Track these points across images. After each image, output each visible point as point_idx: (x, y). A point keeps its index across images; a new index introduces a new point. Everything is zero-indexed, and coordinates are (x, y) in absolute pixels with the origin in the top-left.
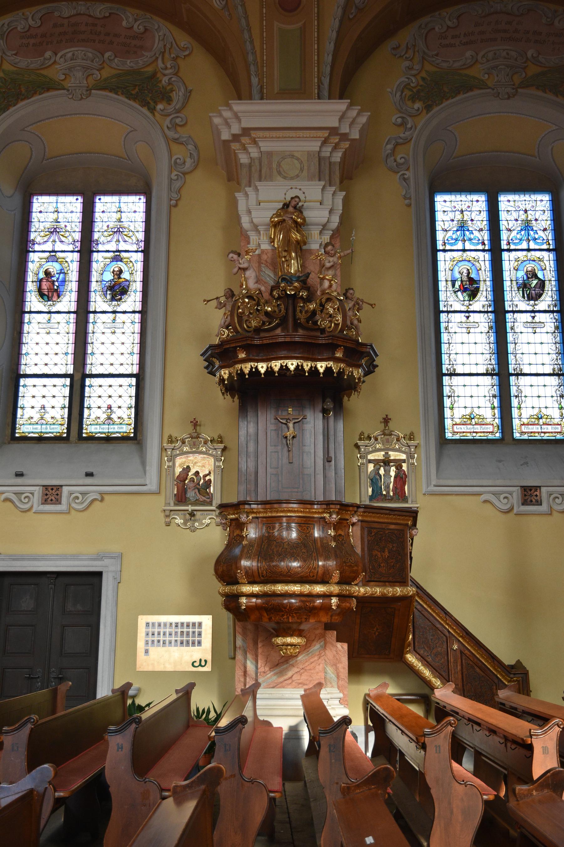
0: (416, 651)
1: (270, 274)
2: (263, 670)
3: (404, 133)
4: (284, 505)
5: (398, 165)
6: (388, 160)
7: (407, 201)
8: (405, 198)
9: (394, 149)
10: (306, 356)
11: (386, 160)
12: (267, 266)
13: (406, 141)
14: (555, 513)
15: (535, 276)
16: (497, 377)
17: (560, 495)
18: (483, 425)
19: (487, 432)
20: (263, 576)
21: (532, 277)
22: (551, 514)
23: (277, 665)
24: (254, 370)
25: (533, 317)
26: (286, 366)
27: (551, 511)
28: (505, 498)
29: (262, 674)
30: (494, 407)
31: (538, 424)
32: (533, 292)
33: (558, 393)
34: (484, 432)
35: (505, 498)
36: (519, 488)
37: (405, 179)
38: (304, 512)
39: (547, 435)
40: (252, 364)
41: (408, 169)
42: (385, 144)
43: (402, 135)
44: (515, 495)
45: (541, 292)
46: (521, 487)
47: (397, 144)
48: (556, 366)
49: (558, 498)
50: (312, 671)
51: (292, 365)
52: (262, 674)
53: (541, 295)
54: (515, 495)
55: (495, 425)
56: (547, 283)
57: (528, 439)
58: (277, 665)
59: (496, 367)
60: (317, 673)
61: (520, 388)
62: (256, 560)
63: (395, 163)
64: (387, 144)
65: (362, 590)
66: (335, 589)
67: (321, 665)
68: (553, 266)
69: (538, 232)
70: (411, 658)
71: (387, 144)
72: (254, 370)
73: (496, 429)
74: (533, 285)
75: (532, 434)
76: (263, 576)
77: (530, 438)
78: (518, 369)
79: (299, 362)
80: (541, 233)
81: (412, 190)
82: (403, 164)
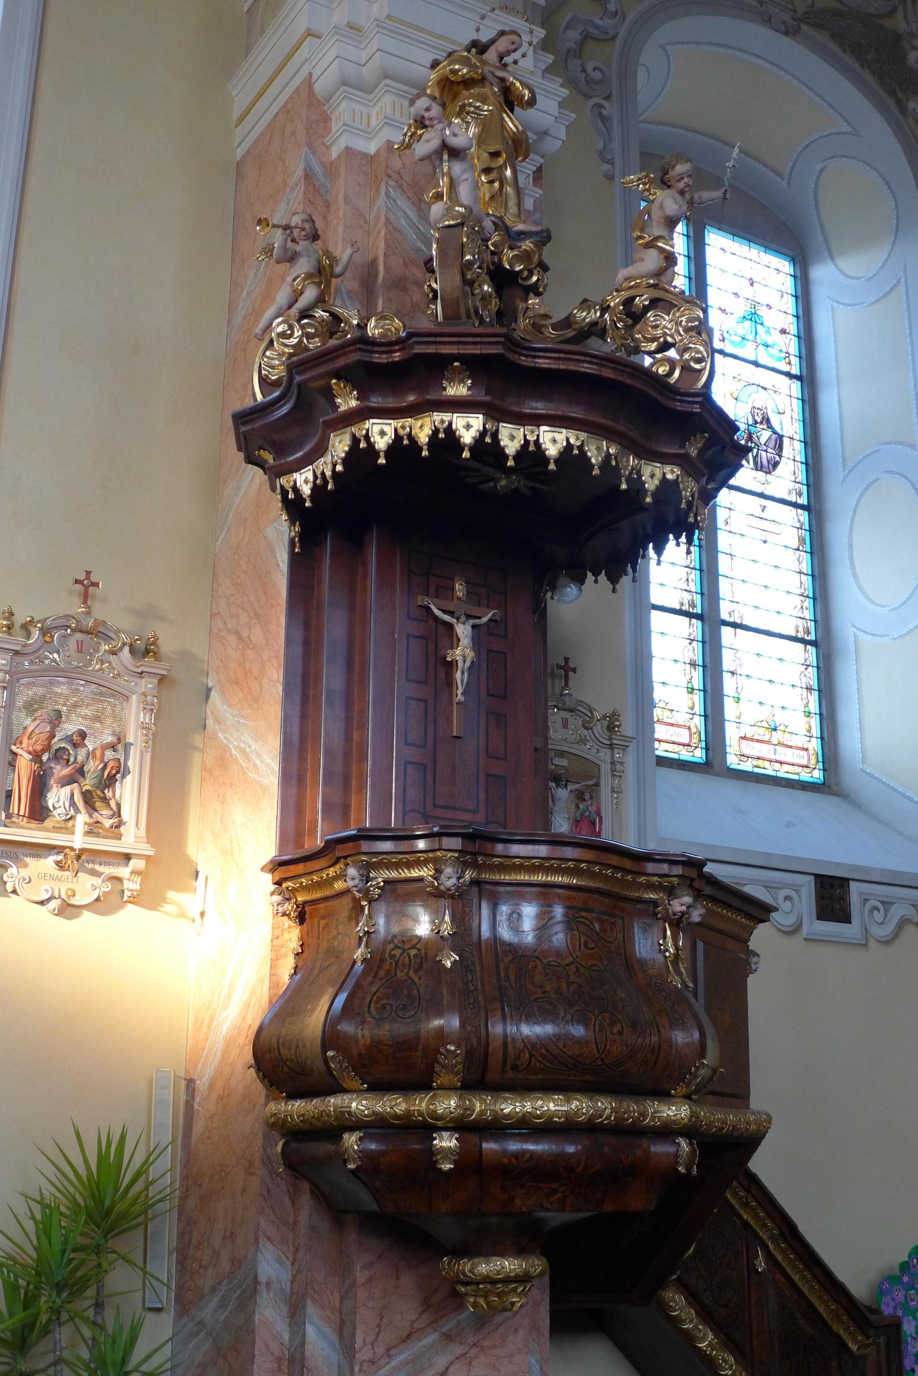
0: (684, 1286)
1: (409, 213)
2: (370, 1355)
3: (601, 19)
4: (500, 848)
5: (589, 80)
6: (570, 62)
7: (606, 167)
8: (603, 159)
9: (582, 44)
10: (594, 418)
11: (566, 62)
12: (401, 187)
13: (606, 37)
14: (872, 944)
15: (767, 421)
16: (700, 623)
17: (882, 902)
18: (672, 725)
19: (680, 744)
20: (515, 1068)
21: (761, 423)
22: (865, 945)
23: (409, 1336)
24: (442, 435)
25: (764, 508)
26: (537, 442)
27: (867, 940)
28: (787, 898)
29: (365, 1365)
30: (693, 689)
31: (768, 742)
32: (764, 454)
33: (804, 680)
34: (673, 743)
35: (787, 898)
36: (812, 878)
37: (603, 118)
38: (589, 874)
39: (786, 768)
40: (438, 417)
41: (608, 98)
42: (563, 26)
43: (597, 21)
44: (804, 892)
45: (777, 458)
46: (817, 876)
47: (586, 37)
48: (800, 622)
49: (878, 910)
50: (498, 1352)
51: (553, 441)
52: (365, 1365)
53: (776, 465)
54: (804, 892)
55: (694, 730)
56: (786, 441)
57: (753, 773)
58: (409, 1336)
59: (698, 599)
60: (512, 1355)
61: (738, 655)
62: (499, 1013)
63: (584, 75)
64: (568, 27)
65: (552, 1106)
66: (448, 1104)
67: (521, 1331)
68: (796, 410)
69: (772, 331)
70: (677, 1302)
71: (568, 27)
72: (442, 435)
73: (695, 740)
74: (763, 440)
75: (760, 763)
76: (515, 1068)
77: (757, 770)
78: (736, 613)
79: (574, 437)
80: (776, 335)
81: (616, 145)
82: (598, 83)
